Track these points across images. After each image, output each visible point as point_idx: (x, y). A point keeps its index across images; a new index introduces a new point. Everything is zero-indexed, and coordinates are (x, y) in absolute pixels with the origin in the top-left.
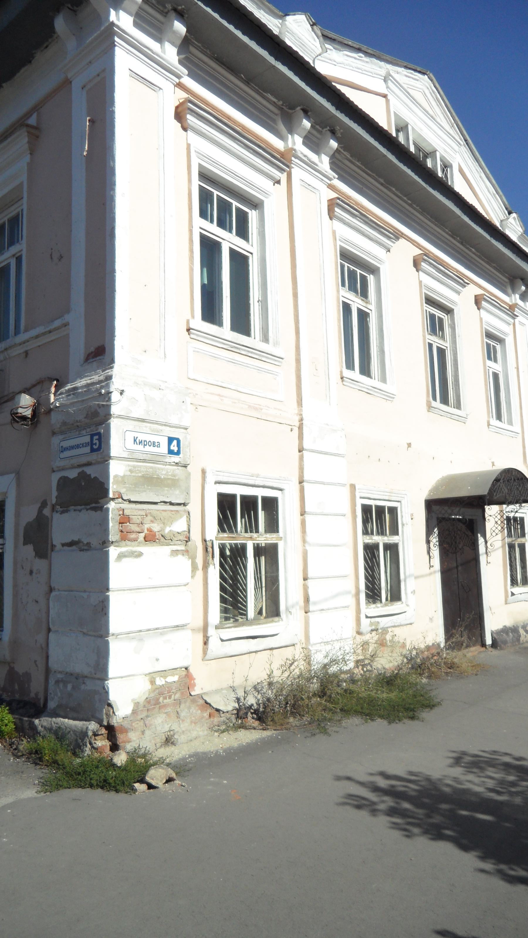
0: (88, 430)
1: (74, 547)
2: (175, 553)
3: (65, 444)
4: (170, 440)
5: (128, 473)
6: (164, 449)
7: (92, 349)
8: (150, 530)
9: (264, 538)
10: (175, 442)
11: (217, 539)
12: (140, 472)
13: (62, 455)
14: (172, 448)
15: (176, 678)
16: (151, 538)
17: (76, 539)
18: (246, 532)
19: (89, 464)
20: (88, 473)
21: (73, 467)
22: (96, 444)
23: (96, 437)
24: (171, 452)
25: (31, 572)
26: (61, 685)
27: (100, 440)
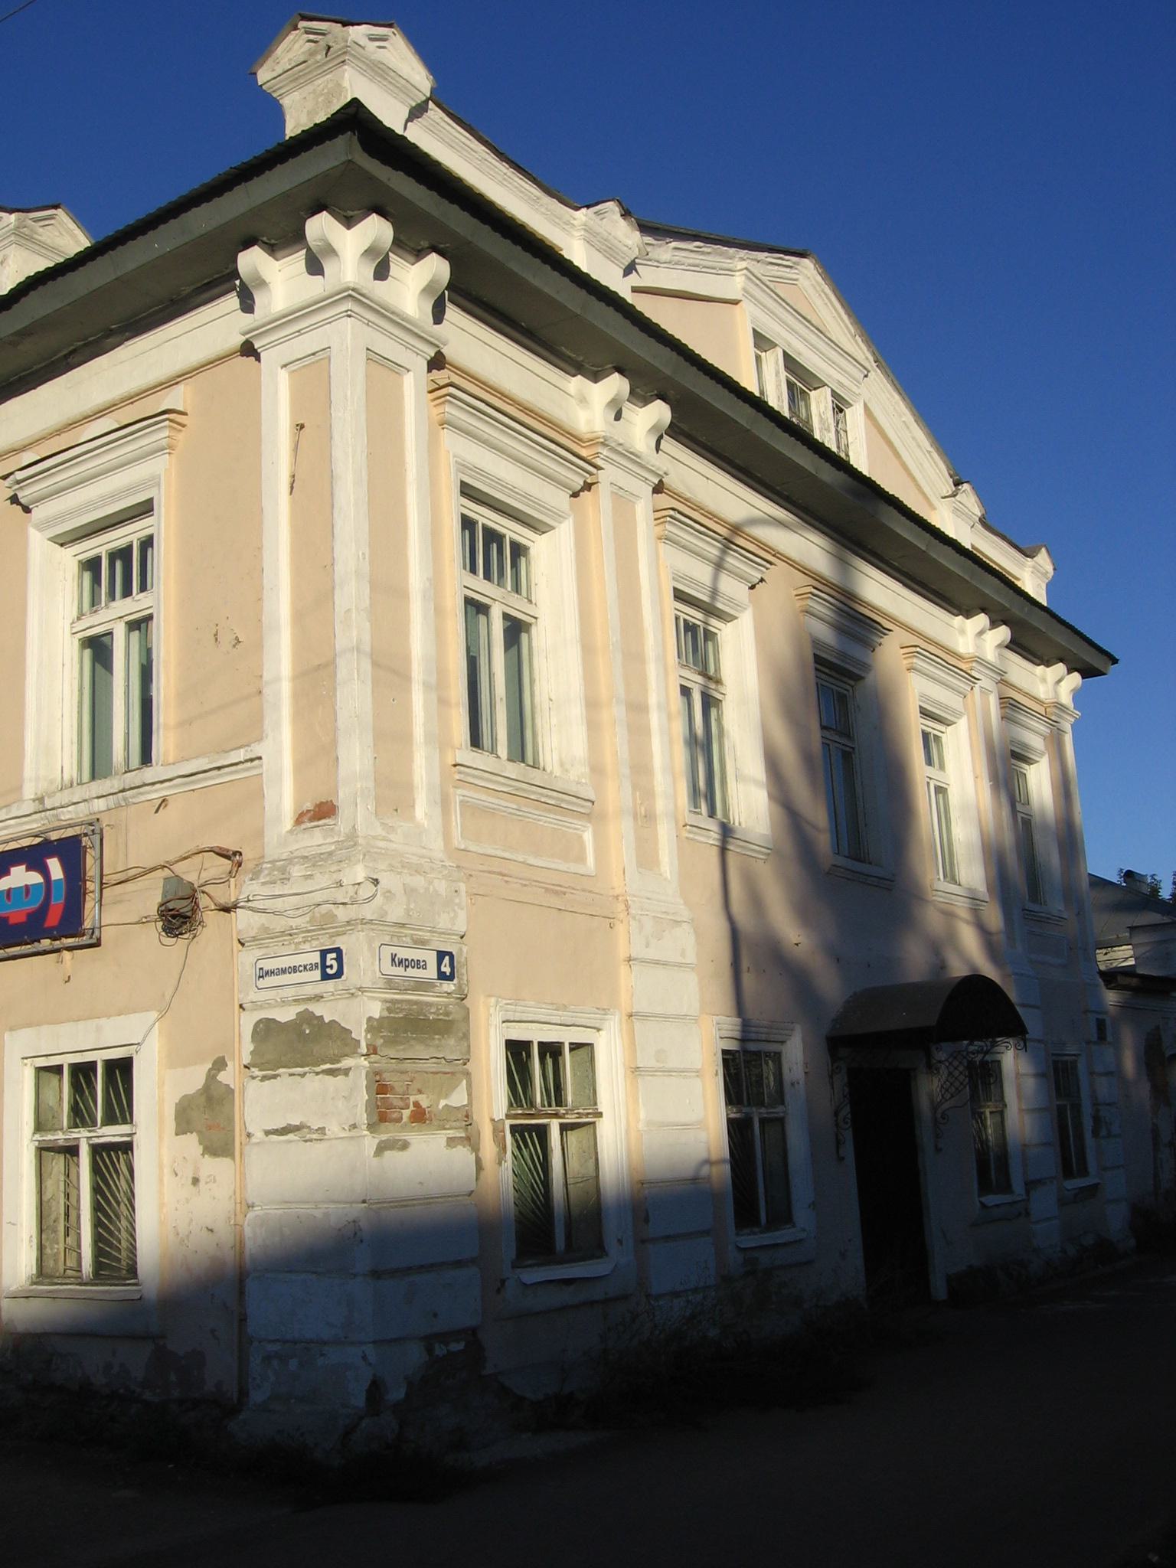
0: (314, 943)
1: (291, 1136)
2: (451, 1142)
3: (268, 965)
4: (441, 955)
5: (386, 1014)
6: (431, 972)
7: (309, 805)
8: (416, 1104)
9: (112, 1133)
10: (447, 958)
11: (508, 1116)
12: (402, 1010)
13: (262, 983)
14: (443, 969)
15: (461, 1346)
16: (420, 1116)
17: (295, 1122)
18: (550, 1105)
19: (318, 998)
20: (318, 1014)
21: (284, 1002)
22: (331, 967)
23: (330, 956)
24: (442, 976)
25: (196, 1181)
26: (275, 1363)
27: (339, 959)
